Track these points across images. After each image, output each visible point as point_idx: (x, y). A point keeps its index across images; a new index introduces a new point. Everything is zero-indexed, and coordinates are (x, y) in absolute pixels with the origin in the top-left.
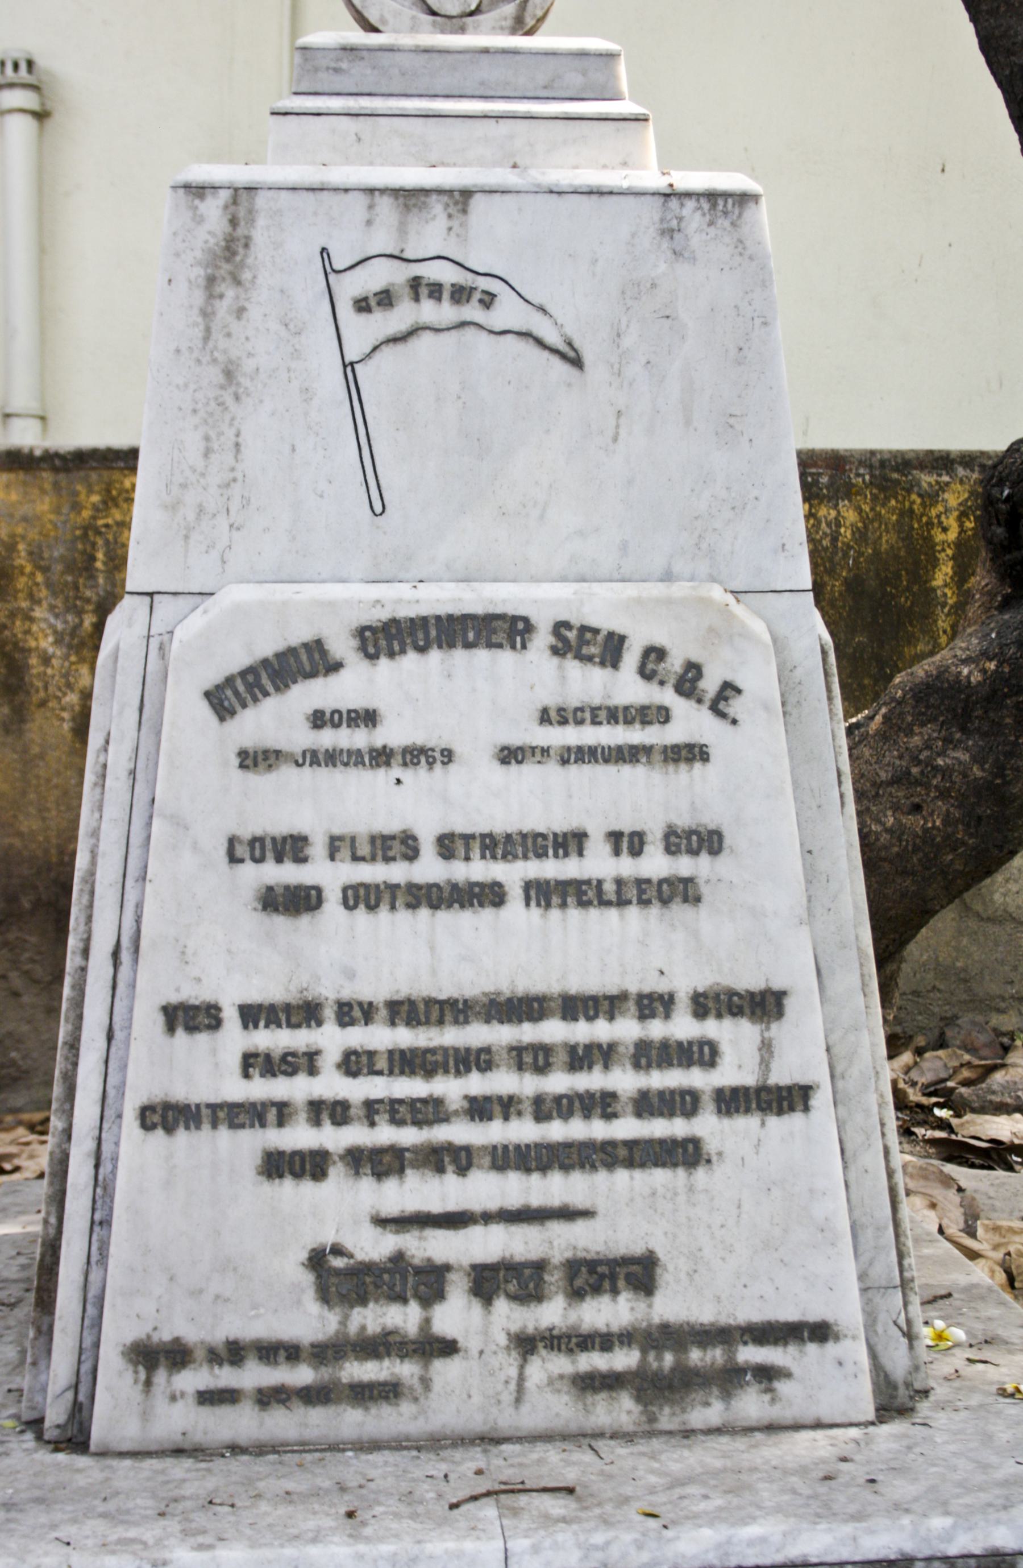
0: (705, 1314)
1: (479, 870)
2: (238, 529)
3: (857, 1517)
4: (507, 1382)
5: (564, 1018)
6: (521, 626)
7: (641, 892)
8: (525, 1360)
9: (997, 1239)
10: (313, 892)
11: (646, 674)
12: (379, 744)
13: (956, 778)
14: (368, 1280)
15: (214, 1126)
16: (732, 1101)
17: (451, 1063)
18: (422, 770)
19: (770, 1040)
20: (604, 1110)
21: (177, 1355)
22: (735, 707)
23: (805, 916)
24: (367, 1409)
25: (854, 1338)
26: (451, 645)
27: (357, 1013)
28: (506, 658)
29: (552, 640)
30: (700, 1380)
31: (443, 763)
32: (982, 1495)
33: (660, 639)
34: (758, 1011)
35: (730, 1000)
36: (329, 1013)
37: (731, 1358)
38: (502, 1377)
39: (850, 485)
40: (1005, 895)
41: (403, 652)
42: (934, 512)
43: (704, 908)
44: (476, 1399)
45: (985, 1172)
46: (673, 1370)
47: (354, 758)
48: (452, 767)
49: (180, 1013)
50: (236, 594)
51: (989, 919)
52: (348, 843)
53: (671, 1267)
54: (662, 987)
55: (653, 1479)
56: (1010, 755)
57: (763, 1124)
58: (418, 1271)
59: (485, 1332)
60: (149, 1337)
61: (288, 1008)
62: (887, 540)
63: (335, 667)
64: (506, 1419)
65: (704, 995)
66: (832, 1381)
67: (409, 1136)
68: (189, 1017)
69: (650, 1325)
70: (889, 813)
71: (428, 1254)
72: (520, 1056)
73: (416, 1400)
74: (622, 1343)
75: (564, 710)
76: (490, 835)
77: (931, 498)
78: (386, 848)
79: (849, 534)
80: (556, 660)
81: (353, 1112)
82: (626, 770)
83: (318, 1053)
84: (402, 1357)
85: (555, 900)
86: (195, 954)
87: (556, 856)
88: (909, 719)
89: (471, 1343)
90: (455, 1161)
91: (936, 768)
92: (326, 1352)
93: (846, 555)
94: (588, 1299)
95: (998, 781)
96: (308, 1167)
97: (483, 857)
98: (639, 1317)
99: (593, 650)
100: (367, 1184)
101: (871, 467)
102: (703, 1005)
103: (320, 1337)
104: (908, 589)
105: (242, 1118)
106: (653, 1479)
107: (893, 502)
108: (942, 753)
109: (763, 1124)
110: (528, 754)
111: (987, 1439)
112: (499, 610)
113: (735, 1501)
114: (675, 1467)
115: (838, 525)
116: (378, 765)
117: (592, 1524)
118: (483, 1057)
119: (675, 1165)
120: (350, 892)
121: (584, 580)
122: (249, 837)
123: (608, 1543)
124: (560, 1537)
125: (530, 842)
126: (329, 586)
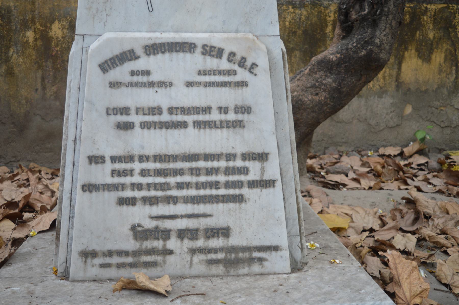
0: (244, 243)
1: (180, 118)
2: (109, 16)
4: (187, 262)
5: (205, 160)
6: (193, 46)
7: (227, 124)
9: (335, 210)
10: (132, 124)
11: (229, 60)
12: (151, 80)
13: (328, 86)
14: (148, 234)
15: (104, 190)
16: (252, 184)
17: (172, 173)
18: (163, 89)
19: (264, 167)
20: (216, 186)
21: (94, 254)
22: (256, 70)
23: (275, 132)
25: (286, 250)
26: (172, 51)
27: (145, 159)
28: (188, 55)
29: (202, 50)
31: (170, 86)
32: (318, 297)
33: (234, 50)
36: (136, 158)
39: (304, 4)
41: (158, 53)
42: (327, 12)
43: (245, 130)
44: (179, 266)
46: (234, 259)
48: (172, 88)
49: (93, 159)
50: (107, 35)
51: (338, 122)
52: (142, 109)
53: (234, 230)
54: (233, 151)
55: (226, 291)
56: (343, 80)
57: (261, 191)
58: (162, 231)
59: (181, 248)
60: (86, 249)
61: (125, 157)
62: (314, 20)
63: (137, 58)
64: (187, 272)
65: (245, 154)
66: (280, 262)
67: (159, 194)
68: (95, 160)
69: (228, 246)
70: (310, 95)
71: (165, 226)
72: (192, 171)
73: (162, 266)
74: (220, 251)
75: (205, 71)
76: (183, 108)
77: (326, 8)
78: (153, 111)
80: (203, 56)
81: (143, 187)
82: (223, 89)
84: (158, 255)
85: (202, 126)
87: (203, 114)
88: (316, 70)
89: (178, 251)
90: (173, 201)
91: (322, 83)
92: (135, 254)
93: (303, 24)
94: (211, 239)
95: (339, 87)
96: (131, 202)
97: (181, 114)
98: (225, 244)
99: (214, 53)
100: (147, 207)
102: (245, 157)
104: (320, 33)
105: (111, 188)
106: (226, 291)
108: (325, 79)
109: (261, 191)
110: (195, 84)
112: (186, 41)
114: (233, 287)
115: (301, 15)
116: (150, 87)
118: (181, 171)
119: (236, 202)
120: (142, 124)
122: (113, 108)
125: (195, 109)
126: (136, 33)
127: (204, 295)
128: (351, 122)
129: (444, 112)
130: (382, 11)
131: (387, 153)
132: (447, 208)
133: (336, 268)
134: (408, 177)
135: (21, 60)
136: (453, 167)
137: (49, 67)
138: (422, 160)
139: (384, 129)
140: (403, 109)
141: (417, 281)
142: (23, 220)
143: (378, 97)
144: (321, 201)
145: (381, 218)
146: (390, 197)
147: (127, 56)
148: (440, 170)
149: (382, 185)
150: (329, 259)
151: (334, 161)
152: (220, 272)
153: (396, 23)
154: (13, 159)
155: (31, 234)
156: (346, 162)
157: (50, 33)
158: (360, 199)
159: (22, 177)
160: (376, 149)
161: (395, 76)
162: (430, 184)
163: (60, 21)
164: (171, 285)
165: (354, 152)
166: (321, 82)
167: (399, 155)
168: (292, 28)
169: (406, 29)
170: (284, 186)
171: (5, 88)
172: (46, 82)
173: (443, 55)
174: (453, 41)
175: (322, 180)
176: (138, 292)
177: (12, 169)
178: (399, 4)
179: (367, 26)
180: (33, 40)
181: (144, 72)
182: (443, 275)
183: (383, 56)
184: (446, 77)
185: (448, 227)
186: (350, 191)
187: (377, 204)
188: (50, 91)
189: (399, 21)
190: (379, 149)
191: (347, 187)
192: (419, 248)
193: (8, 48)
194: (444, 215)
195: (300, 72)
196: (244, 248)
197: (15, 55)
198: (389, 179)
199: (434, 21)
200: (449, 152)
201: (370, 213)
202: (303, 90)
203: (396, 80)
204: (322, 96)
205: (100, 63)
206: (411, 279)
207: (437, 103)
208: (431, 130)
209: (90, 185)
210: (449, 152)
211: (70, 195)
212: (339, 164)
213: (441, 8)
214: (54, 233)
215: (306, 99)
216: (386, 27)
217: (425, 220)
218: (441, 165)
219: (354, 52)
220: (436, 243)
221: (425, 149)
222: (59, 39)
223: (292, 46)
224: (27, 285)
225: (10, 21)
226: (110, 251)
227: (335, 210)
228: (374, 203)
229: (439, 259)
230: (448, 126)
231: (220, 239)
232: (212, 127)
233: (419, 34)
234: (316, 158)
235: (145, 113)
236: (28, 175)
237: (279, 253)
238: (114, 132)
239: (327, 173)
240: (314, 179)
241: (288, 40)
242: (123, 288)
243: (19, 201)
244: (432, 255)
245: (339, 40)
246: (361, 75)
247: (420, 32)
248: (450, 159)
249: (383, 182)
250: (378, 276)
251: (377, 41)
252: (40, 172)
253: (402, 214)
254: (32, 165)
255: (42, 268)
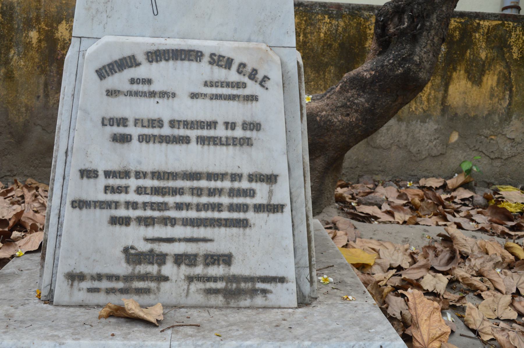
0: (246, 272)
1: (182, 132)
3: (282, 340)
5: (207, 180)
6: (199, 54)
7: (234, 141)
8: (190, 284)
9: (361, 244)
11: (239, 72)
12: (152, 90)
13: (361, 107)
14: (142, 257)
15: (95, 208)
16: (259, 208)
17: (171, 192)
18: (165, 99)
19: (272, 190)
21: (81, 277)
22: (268, 84)
23: (286, 152)
24: (140, 296)
26: (177, 59)
27: (141, 175)
28: (194, 64)
29: (209, 59)
30: (243, 292)
33: (244, 61)
34: (269, 181)
35: (260, 177)
36: (132, 174)
37: (254, 286)
38: (182, 288)
39: (342, 14)
40: (380, 140)
41: (161, 60)
42: (367, 24)
43: (253, 148)
44: (174, 295)
45: (362, 223)
46: (235, 289)
47: (143, 94)
49: (85, 172)
50: (107, 39)
51: (374, 147)
53: (237, 258)
54: (239, 171)
55: (223, 323)
56: (377, 100)
57: (268, 216)
58: (158, 255)
59: (178, 275)
60: (72, 271)
61: (120, 172)
62: (353, 32)
63: (138, 64)
64: (183, 301)
65: (252, 175)
66: (285, 295)
67: (156, 214)
68: (88, 174)
72: (193, 191)
73: (155, 294)
74: (220, 280)
76: (186, 121)
77: (367, 19)
78: (153, 124)
79: (341, 29)
80: (210, 66)
81: (139, 205)
82: (231, 102)
83: (128, 187)
84: (151, 281)
85: (206, 143)
86: (90, 154)
87: (207, 129)
89: (173, 278)
90: (171, 222)
91: (354, 103)
92: (127, 278)
93: (340, 36)
94: (210, 266)
97: (184, 128)
99: (222, 63)
100: (142, 228)
101: (349, 9)
102: (251, 178)
103: (126, 273)
104: (358, 47)
106: (223, 323)
107: (355, 20)
108: (357, 99)
109: (268, 216)
111: (330, 315)
112: (192, 49)
113: (246, 332)
114: (231, 319)
115: (338, 27)
116: (151, 97)
117: (199, 338)
119: (240, 227)
120: (141, 137)
121: (222, 40)
123: (202, 344)
124: (188, 342)
127: (199, 326)
128: (390, 148)
129: (494, 142)
130: (423, 25)
131: (428, 185)
132: (486, 247)
133: (348, 305)
134: (449, 213)
135: (22, 63)
136: (501, 204)
137: (53, 72)
138: (467, 194)
139: (426, 158)
140: (448, 137)
141: (437, 323)
142: (10, 239)
143: (421, 122)
144: (346, 234)
145: (412, 255)
146: (425, 233)
147: (127, 62)
148: (485, 207)
149: (418, 219)
150: (342, 295)
151: (368, 190)
152: (220, 302)
153: (438, 40)
154: (9, 174)
155: (17, 254)
156: (381, 192)
157: (57, 34)
158: (391, 234)
159: (17, 193)
160: (417, 180)
161: (441, 99)
162: (473, 221)
163: (68, 21)
164: (164, 314)
165: (391, 182)
166: (352, 101)
167: (441, 187)
168: (328, 40)
169: (455, 46)
170: (294, 212)
171: (3, 94)
172: (49, 89)
173: (496, 78)
174: (507, 63)
175: (352, 211)
176: (127, 320)
177: (7, 184)
178: (443, 18)
179: (406, 41)
180: (37, 41)
181: (145, 81)
182: (472, 319)
183: (422, 75)
184: (498, 102)
185: (485, 269)
186: (381, 224)
187: (410, 240)
188: (53, 98)
189: (442, 37)
190: (420, 179)
191: (379, 220)
192: (450, 290)
193: (8, 48)
194: (483, 255)
195: (331, 89)
196: (246, 278)
197: (15, 57)
198: (427, 213)
199: (487, 39)
200: (498, 186)
201: (399, 249)
202: (332, 110)
203: (442, 104)
204: (354, 117)
205: (97, 68)
206: (431, 321)
207: (486, 132)
208: (479, 161)
209: (80, 201)
210: (498, 186)
211: (58, 212)
212: (372, 195)
213: (495, 25)
214: (39, 254)
215: (335, 120)
216: (427, 43)
217: (461, 260)
218: (488, 201)
219: (390, 70)
220: (470, 285)
221: (471, 182)
222: (66, 42)
223: (326, 60)
224: (6, 307)
225: (12, 18)
226: (99, 274)
227: (361, 244)
228: (407, 239)
229: (469, 303)
230: (499, 158)
231: (221, 267)
232: (217, 144)
233: (470, 53)
234: (348, 187)
235: (144, 125)
236: (23, 191)
237: (285, 285)
238: (109, 144)
239: (358, 204)
240: (342, 210)
241: (322, 54)
242: (110, 315)
243: (10, 219)
244: (463, 297)
245: (374, 55)
246: (398, 96)
247: (471, 51)
248: (499, 194)
249: (420, 217)
250: (399, 317)
251: (416, 58)
252: (37, 188)
253: (436, 252)
254: (29, 181)
255: (25, 290)
